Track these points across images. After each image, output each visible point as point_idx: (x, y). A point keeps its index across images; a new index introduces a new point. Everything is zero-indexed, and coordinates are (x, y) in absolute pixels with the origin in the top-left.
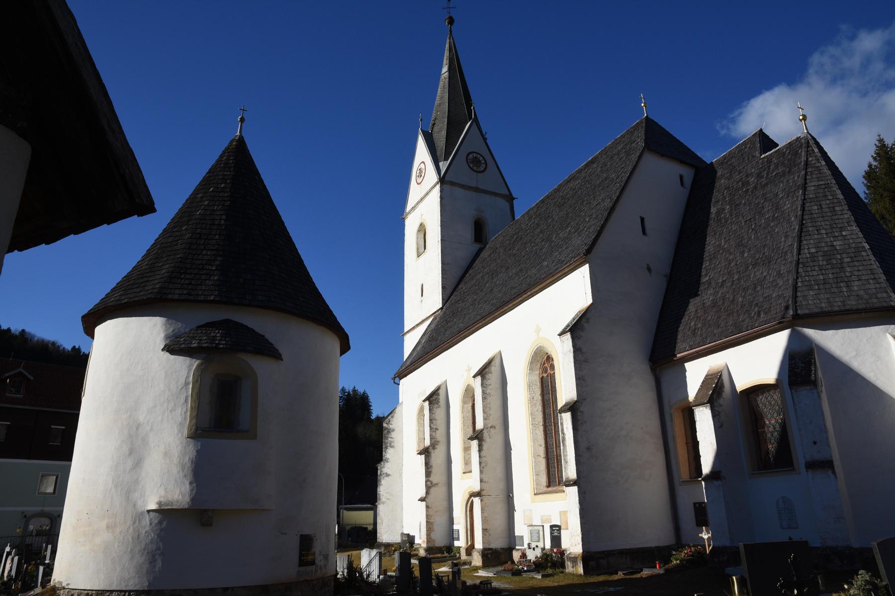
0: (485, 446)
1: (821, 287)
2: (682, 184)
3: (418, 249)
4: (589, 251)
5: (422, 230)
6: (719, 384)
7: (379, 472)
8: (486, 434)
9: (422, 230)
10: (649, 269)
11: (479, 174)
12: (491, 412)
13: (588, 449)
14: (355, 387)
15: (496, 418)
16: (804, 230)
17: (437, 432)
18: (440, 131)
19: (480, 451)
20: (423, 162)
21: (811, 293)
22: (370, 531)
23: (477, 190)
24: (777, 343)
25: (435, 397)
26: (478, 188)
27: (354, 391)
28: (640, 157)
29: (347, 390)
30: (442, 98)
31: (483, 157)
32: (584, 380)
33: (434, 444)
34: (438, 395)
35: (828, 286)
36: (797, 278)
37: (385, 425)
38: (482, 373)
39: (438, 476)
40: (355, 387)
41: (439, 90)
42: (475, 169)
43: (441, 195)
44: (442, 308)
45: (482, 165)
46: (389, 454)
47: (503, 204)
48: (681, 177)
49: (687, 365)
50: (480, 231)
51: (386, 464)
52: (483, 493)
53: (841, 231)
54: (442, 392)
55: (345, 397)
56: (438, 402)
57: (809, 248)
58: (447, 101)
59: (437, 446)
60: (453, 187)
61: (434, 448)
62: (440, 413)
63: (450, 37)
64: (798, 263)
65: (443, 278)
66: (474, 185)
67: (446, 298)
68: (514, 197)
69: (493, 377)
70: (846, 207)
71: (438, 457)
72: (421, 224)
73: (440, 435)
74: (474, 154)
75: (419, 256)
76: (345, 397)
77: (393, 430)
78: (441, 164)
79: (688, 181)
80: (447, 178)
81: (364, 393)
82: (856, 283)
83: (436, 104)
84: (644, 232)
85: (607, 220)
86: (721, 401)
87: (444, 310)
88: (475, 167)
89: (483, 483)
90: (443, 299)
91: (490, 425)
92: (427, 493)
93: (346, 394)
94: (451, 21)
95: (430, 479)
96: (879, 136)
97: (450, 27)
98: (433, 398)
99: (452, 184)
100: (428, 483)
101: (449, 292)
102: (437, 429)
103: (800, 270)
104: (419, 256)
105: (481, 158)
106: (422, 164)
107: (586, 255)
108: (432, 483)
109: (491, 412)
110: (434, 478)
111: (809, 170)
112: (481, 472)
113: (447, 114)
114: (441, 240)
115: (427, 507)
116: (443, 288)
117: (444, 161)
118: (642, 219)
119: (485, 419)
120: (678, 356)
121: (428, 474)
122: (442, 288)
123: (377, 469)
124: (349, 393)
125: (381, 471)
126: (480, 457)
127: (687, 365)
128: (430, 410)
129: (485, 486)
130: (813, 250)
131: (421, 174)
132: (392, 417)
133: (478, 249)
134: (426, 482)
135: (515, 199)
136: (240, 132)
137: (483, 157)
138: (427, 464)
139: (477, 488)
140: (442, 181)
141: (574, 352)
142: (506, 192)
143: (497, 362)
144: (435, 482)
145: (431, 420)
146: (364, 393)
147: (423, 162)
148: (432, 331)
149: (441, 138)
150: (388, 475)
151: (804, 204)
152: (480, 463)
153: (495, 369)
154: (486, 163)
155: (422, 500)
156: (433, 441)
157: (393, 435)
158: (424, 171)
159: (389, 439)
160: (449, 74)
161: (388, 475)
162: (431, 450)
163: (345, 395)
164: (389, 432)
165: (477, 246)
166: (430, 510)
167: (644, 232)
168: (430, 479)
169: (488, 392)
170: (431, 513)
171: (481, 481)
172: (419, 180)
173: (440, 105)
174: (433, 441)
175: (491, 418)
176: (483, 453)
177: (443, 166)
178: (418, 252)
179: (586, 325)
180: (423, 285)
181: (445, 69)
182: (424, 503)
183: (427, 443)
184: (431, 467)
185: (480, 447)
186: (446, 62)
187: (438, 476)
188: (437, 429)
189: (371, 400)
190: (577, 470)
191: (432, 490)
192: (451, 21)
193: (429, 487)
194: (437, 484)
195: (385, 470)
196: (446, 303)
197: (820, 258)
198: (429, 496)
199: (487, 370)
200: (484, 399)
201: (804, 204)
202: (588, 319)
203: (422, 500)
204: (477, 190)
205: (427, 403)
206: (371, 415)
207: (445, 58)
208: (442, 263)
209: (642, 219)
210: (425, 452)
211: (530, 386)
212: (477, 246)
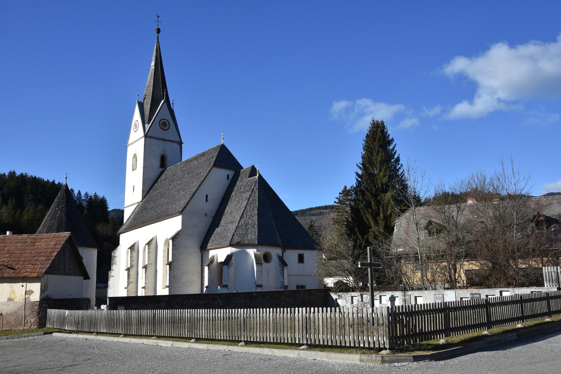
0: (148, 271)
1: (240, 236)
2: (228, 179)
3: (133, 166)
4: (182, 211)
5: (135, 156)
6: (213, 260)
7: (109, 275)
8: (148, 267)
9: (135, 156)
10: (206, 215)
11: (166, 131)
12: (151, 258)
13: (174, 277)
14: (96, 193)
15: (152, 261)
16: (243, 215)
17: (133, 262)
18: (147, 104)
19: (145, 272)
20: (137, 121)
21: (237, 237)
22: (312, 307)
23: (163, 140)
24: (228, 251)
25: (133, 247)
26: (164, 139)
27: (96, 196)
28: (212, 167)
29: (89, 195)
30: (150, 82)
31: (168, 121)
32: (175, 255)
33: (132, 266)
34: (135, 246)
35: (242, 235)
36: (235, 232)
37: (112, 254)
38: (149, 244)
39: (132, 279)
40: (96, 193)
41: (149, 76)
42: (163, 128)
43: (144, 144)
44: (141, 201)
45: (167, 126)
46: (114, 267)
47: (177, 146)
48: (228, 176)
49: (210, 251)
50: (163, 162)
51: (112, 271)
52: (146, 287)
53: (252, 217)
54: (136, 246)
55: (88, 200)
56: (134, 249)
57: (242, 222)
58: (152, 85)
59: (133, 267)
60: (152, 139)
61: (131, 268)
62: (135, 254)
63: (157, 42)
64: (237, 227)
65: (143, 186)
66: (162, 137)
67: (144, 196)
68: (183, 142)
69: (153, 245)
70: (257, 209)
71: (133, 272)
72: (135, 154)
73: (134, 263)
74: (163, 120)
75: (133, 170)
76: (88, 200)
77: (116, 257)
78: (146, 125)
79: (230, 178)
80: (148, 135)
81: (103, 198)
82: (250, 235)
83: (146, 85)
84: (207, 201)
85: (191, 199)
86: (212, 265)
87: (142, 202)
88: (164, 127)
89: (146, 284)
90: (142, 197)
91: (150, 263)
92: (128, 286)
93: (89, 198)
94: (158, 31)
95: (129, 280)
96: (373, 118)
97: (158, 35)
98: (132, 248)
99: (151, 137)
100: (128, 282)
101: (145, 193)
102: (133, 260)
103: (237, 229)
104: (133, 170)
105: (167, 122)
106: (137, 122)
107: (181, 213)
108: (130, 282)
109: (151, 258)
110: (131, 280)
111: (253, 192)
112: (145, 280)
113: (151, 94)
114: (143, 167)
115: (128, 291)
116: (143, 191)
117: (148, 124)
118: (207, 196)
119: (148, 261)
120: (208, 248)
121: (129, 278)
122: (142, 191)
123: (108, 274)
124: (91, 197)
125: (110, 275)
126: (145, 274)
127: (210, 251)
128: (131, 253)
129: (147, 285)
130: (243, 223)
131: (136, 126)
132: (116, 251)
133: (161, 171)
134: (128, 281)
135: (183, 143)
136: (66, 182)
137: (168, 121)
138: (128, 274)
139: (144, 286)
140: (146, 136)
141: (172, 246)
142: (178, 140)
143: (154, 240)
144: (131, 281)
145: (131, 257)
146: (103, 198)
147: (135, 132)
148: (136, 213)
149: (147, 107)
150: (113, 276)
151: (246, 206)
152: (145, 277)
153: (153, 242)
154: (169, 125)
155: (126, 288)
156: (131, 265)
157: (116, 259)
158: (138, 126)
159: (114, 261)
160: (155, 67)
161: (113, 276)
162: (130, 269)
163: (88, 199)
164: (114, 258)
165: (161, 169)
166: (129, 292)
167: (207, 201)
168: (129, 280)
169: (150, 251)
170: (129, 294)
171: (145, 283)
172: (136, 130)
173: (148, 87)
174: (131, 265)
175: (151, 261)
176: (147, 273)
177: (147, 126)
178: (133, 168)
179: (178, 237)
180: (134, 186)
181: (153, 63)
182: (126, 289)
183: (129, 266)
184: (130, 275)
185: (146, 271)
186: (154, 58)
187: (132, 279)
188: (133, 260)
189: (108, 204)
190: (169, 283)
191: (130, 285)
192: (158, 31)
193: (129, 283)
194: (132, 282)
195: (112, 274)
196: (144, 198)
197: (244, 226)
198: (128, 287)
199: (150, 243)
200: (148, 253)
201: (246, 206)
202: (179, 235)
203: (126, 288)
204: (163, 140)
205: (130, 250)
206: (108, 208)
207: (153, 56)
208: (143, 179)
209: (207, 196)
210: (128, 270)
211: (164, 251)
212: (161, 169)
